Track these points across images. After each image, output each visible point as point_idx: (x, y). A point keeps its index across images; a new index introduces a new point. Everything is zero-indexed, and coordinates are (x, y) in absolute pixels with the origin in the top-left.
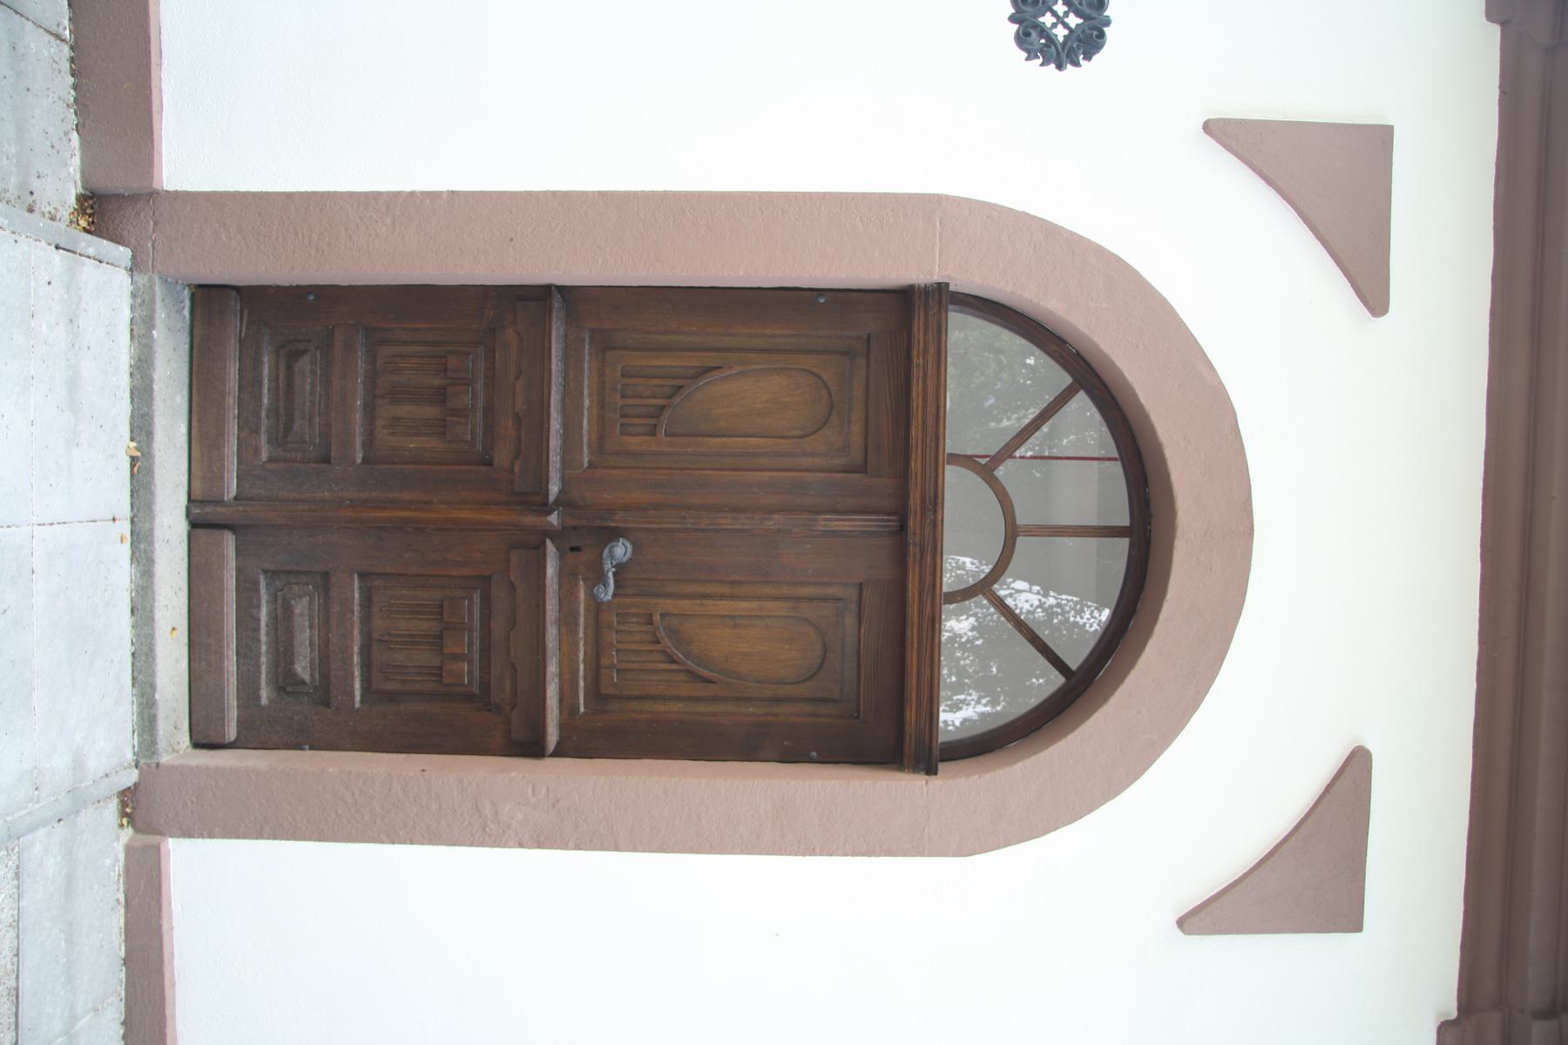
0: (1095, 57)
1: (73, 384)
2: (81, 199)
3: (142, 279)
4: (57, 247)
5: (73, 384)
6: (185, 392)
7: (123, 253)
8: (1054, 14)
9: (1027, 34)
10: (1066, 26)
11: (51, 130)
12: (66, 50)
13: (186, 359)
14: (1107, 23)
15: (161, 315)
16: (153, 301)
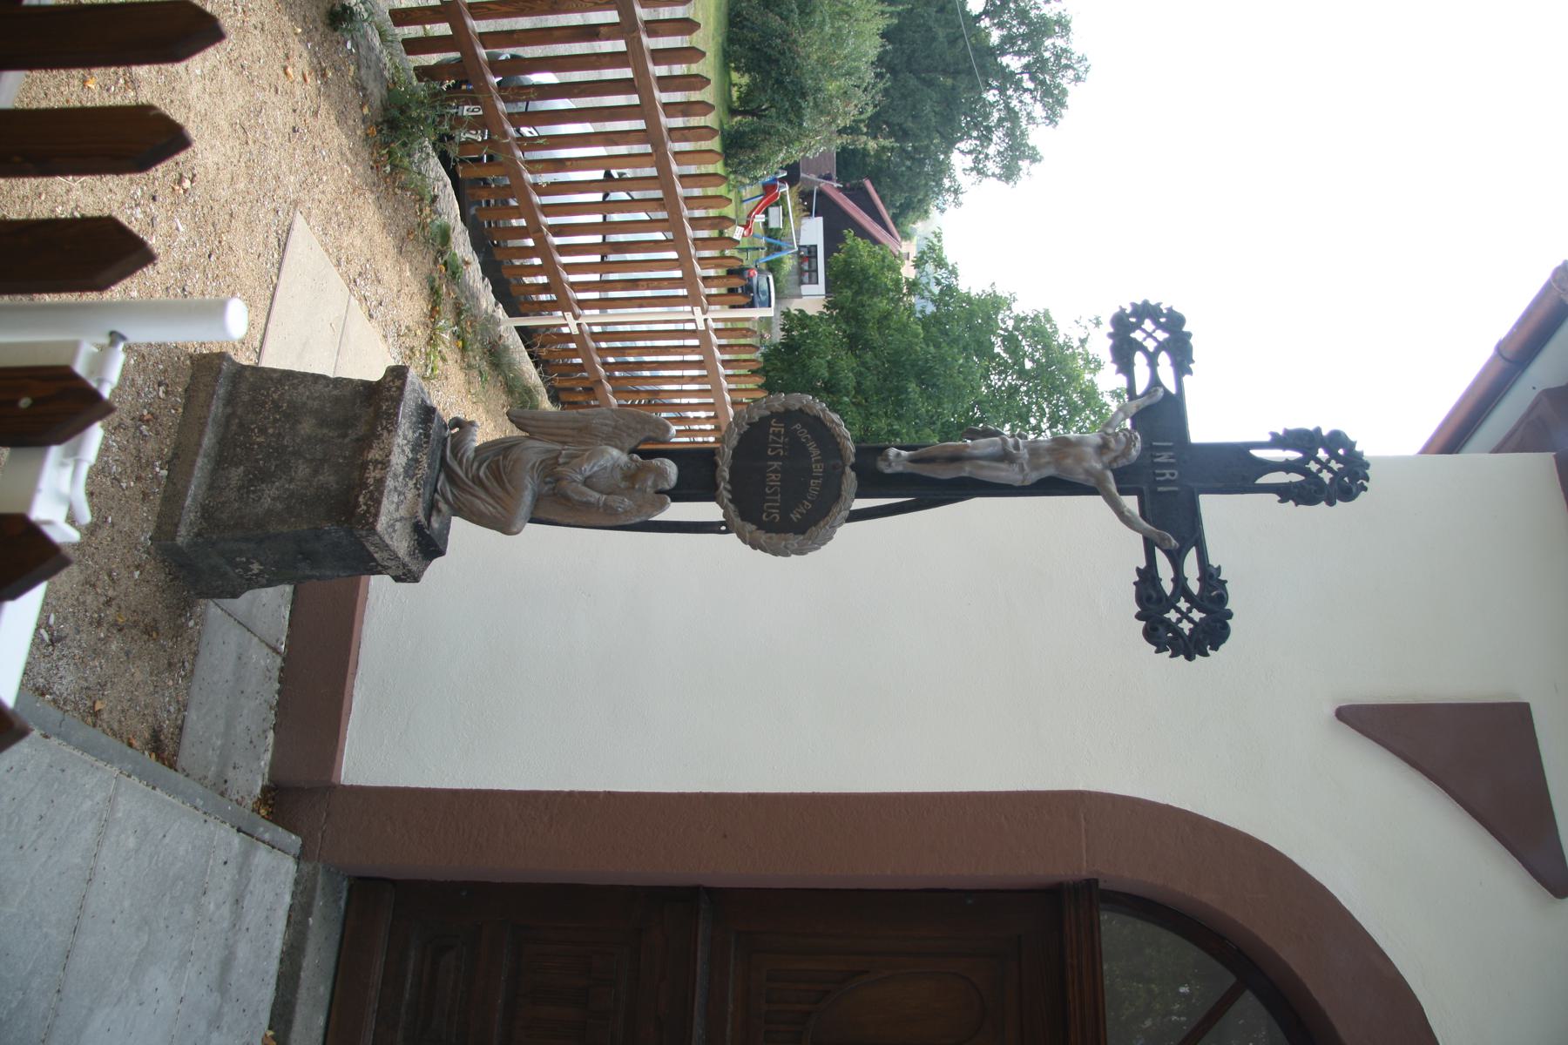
0: (1222, 647)
1: (227, 964)
2: (265, 790)
3: (307, 867)
4: (239, 830)
5: (227, 964)
6: (329, 983)
7: (294, 841)
8: (1178, 610)
9: (1156, 629)
10: (1191, 620)
11: (253, 728)
12: (279, 660)
13: (335, 949)
14: (1230, 615)
15: (319, 903)
16: (314, 889)
